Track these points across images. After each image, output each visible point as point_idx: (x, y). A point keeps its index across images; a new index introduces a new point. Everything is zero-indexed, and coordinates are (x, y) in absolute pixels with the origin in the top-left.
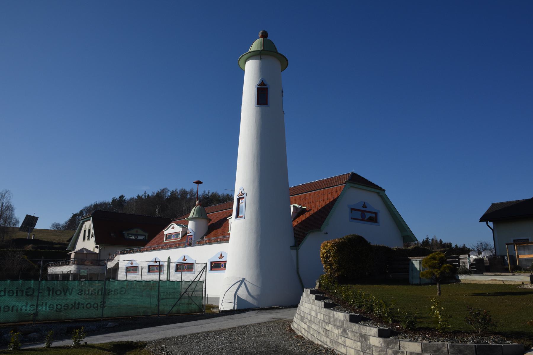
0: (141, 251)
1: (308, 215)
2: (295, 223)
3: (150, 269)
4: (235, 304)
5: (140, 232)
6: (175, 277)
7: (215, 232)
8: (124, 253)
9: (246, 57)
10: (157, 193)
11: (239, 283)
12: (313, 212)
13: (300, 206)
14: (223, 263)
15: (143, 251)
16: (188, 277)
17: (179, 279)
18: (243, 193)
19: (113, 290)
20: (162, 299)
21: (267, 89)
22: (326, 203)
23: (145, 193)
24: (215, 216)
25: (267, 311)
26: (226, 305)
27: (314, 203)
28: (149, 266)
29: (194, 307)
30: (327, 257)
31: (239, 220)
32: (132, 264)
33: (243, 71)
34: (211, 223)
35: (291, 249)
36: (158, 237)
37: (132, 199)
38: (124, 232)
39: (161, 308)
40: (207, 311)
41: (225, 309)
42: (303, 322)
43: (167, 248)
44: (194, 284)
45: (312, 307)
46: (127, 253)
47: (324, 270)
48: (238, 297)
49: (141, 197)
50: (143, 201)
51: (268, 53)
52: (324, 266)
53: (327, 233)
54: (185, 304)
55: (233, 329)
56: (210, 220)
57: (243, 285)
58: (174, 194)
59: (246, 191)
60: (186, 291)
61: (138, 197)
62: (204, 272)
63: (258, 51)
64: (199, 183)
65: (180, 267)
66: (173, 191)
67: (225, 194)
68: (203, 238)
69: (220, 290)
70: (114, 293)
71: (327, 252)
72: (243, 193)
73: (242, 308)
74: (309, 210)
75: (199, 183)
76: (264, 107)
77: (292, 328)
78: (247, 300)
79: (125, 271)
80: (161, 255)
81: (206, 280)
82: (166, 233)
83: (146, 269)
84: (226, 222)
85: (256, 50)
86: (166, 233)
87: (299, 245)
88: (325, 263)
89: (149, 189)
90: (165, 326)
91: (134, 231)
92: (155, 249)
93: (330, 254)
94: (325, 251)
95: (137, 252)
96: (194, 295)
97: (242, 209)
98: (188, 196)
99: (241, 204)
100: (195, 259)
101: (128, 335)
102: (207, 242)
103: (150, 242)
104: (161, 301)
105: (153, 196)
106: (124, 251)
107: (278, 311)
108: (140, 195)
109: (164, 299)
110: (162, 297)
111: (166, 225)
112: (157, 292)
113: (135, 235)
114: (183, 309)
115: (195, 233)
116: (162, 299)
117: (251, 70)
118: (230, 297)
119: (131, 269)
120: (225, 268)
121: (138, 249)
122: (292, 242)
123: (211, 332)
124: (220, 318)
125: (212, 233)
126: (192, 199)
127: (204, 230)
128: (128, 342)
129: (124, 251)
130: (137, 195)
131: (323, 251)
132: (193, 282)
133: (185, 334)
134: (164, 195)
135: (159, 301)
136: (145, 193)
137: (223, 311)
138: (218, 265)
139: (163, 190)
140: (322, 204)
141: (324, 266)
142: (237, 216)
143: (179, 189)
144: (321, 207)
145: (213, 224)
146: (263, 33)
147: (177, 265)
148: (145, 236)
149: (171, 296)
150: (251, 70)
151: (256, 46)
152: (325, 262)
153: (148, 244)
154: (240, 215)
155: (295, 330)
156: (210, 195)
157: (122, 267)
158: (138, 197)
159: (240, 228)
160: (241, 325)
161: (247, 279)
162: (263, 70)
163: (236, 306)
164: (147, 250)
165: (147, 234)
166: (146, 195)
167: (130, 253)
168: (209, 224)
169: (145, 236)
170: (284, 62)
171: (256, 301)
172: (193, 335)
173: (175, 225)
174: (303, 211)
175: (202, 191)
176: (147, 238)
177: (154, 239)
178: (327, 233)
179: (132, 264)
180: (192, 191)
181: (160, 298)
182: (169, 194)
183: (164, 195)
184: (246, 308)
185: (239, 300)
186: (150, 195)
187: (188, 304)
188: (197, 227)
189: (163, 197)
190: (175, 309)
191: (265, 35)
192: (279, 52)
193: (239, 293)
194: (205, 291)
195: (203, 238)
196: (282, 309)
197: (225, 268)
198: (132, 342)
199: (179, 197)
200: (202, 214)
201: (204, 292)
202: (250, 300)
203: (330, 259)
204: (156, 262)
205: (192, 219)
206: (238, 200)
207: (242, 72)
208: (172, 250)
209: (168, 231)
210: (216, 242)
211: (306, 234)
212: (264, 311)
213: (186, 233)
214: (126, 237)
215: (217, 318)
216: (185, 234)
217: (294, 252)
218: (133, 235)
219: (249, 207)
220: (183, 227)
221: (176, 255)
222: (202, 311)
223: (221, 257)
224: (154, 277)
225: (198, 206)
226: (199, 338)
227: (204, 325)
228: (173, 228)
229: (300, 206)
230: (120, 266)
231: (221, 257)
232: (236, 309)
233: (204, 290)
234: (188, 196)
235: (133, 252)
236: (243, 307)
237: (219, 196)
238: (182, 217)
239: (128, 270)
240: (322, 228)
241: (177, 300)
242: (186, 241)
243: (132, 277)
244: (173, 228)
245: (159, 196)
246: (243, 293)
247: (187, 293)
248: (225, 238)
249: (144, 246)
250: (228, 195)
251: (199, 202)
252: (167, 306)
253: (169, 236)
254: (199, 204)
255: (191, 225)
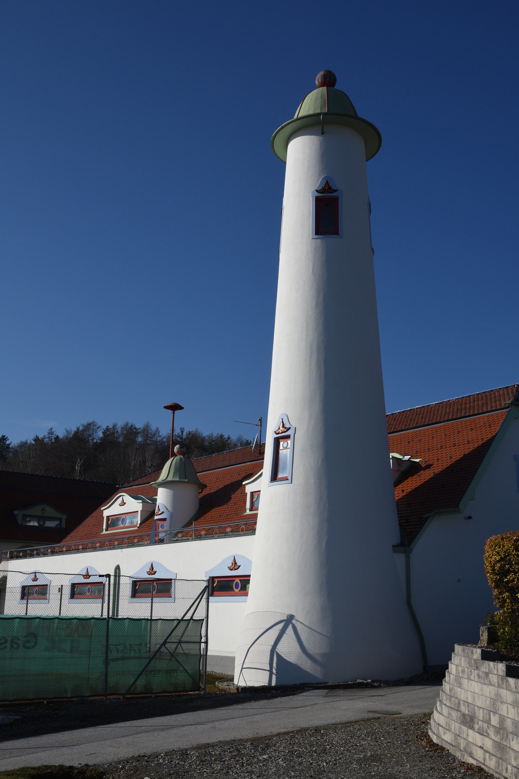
0: (54, 553)
1: (425, 476)
2: (399, 493)
3: (77, 591)
4: (271, 671)
5: (50, 511)
6: (132, 609)
7: (215, 512)
8: (18, 557)
9: (288, 130)
10: (76, 433)
11: (280, 626)
12: (437, 469)
13: (407, 458)
14: (237, 580)
15: (60, 552)
16: (165, 609)
17: (146, 615)
18: (287, 426)
19: (9, 639)
20: (114, 660)
21: (336, 199)
22: (467, 452)
23: (51, 432)
24: (214, 478)
25: (349, 693)
26: (252, 674)
27: (441, 452)
28: (73, 586)
29: (181, 678)
30: (504, 573)
31: (279, 487)
32: (35, 579)
33: (283, 164)
34: (206, 492)
35: (395, 552)
36: (89, 522)
37: (23, 445)
38: (16, 512)
39: (112, 680)
40: (209, 688)
41: (250, 684)
42: (472, 728)
43: (112, 547)
44: (183, 625)
45: (498, 695)
46: (25, 556)
47: (496, 603)
48: (279, 657)
49: (43, 439)
50: (47, 449)
51: (336, 121)
52: (496, 592)
53: (470, 518)
54: (169, 675)
55: (291, 735)
56: (203, 486)
57: (290, 629)
58: (110, 433)
59: (293, 423)
60: (165, 642)
61: (37, 439)
62: (204, 601)
63: (318, 115)
64: (175, 407)
65: (142, 588)
66: (107, 429)
67: (215, 435)
68: (189, 524)
69: (239, 640)
70: (12, 647)
71: (502, 559)
72: (287, 426)
73: (287, 684)
74: (428, 467)
75: (175, 407)
76: (333, 239)
77: (435, 740)
78: (299, 663)
79: (19, 595)
80: (99, 562)
81: (207, 617)
82: (106, 513)
83: (67, 591)
84: (238, 492)
85: (311, 112)
86: (106, 513)
87: (410, 543)
88: (497, 586)
89: (61, 424)
90: (128, 724)
91: (36, 510)
92: (85, 549)
93: (510, 564)
94: (498, 558)
95: (45, 554)
96: (180, 650)
97: (285, 462)
98: (140, 439)
99: (285, 452)
100: (175, 571)
101: (51, 747)
102: (203, 533)
103: (73, 534)
104: (112, 665)
105: (66, 438)
106: (32, 550)
107: (373, 692)
108: (41, 437)
109: (117, 659)
110: (113, 654)
111: (106, 495)
112: (104, 643)
113: (40, 518)
114: (158, 682)
115: (172, 515)
116: (114, 660)
117: (300, 161)
118: (261, 656)
119: (33, 591)
120: (251, 591)
121: (49, 547)
122: (395, 537)
123: (241, 742)
124: (247, 705)
125: (208, 515)
126: (148, 445)
127: (191, 507)
128: (61, 767)
129: (19, 552)
130: (33, 436)
131: (491, 556)
132: (179, 621)
133: (183, 744)
134: (89, 436)
135: (107, 663)
136: (51, 432)
137: (246, 690)
138: (227, 585)
139: (89, 427)
140: (457, 454)
141: (496, 592)
142: (274, 478)
143: (120, 424)
144: (454, 460)
145: (210, 495)
146: (324, 76)
147: (135, 583)
148: (60, 520)
149: (132, 654)
150: (300, 161)
151: (310, 104)
152: (498, 584)
153: (68, 538)
154: (280, 476)
155: (447, 747)
156: (184, 436)
157: (14, 585)
158: (37, 439)
159: (279, 502)
160: (304, 725)
161: (300, 616)
162: (328, 159)
163: (274, 677)
164: (69, 551)
165: (64, 517)
166: (53, 436)
167: (31, 556)
168: (201, 495)
169: (60, 520)
170: (372, 138)
171: (319, 668)
172: (204, 748)
173: (127, 498)
174: (412, 469)
175: (187, 423)
176: (64, 526)
177: (81, 526)
178: (470, 518)
179: (35, 579)
180: (146, 429)
181: (110, 657)
182: (100, 434)
183: (89, 436)
184: (298, 682)
185: (280, 664)
186: (61, 436)
187: (170, 672)
188: (175, 500)
189: (88, 441)
190: (141, 682)
191: (329, 81)
192: (360, 115)
193: (283, 649)
194: (206, 643)
195: (189, 524)
196: (379, 687)
197: (251, 591)
198: (71, 768)
199: (121, 439)
200: (186, 474)
201: (203, 646)
202: (306, 665)
203: (511, 576)
204: (87, 576)
205: (165, 484)
206: (277, 442)
207: (279, 166)
208: (124, 550)
209: (112, 510)
210: (223, 534)
211: (426, 519)
212: (341, 692)
213: (153, 514)
214: (20, 521)
215: (240, 706)
216: (149, 515)
217: (400, 558)
218: (34, 517)
219: (300, 457)
220: (144, 502)
221: (134, 561)
222: (199, 689)
223: (235, 566)
224: (90, 609)
225: (178, 457)
226: (220, 758)
227: (217, 724)
228: (123, 504)
229: (407, 458)
230: (9, 584)
231: (235, 566)
232: (273, 684)
233: (203, 640)
234: (140, 439)
235: (38, 555)
236: (289, 681)
237: (203, 439)
238: (140, 481)
239: (26, 592)
240: (461, 505)
241: (145, 662)
242: (148, 531)
243: (38, 609)
244: (123, 504)
245: (79, 439)
246: (289, 649)
247: (167, 645)
248: (248, 527)
249: (59, 541)
250: (222, 436)
251: (180, 448)
252: (125, 676)
253: (113, 521)
254: (180, 452)
255: (162, 496)
